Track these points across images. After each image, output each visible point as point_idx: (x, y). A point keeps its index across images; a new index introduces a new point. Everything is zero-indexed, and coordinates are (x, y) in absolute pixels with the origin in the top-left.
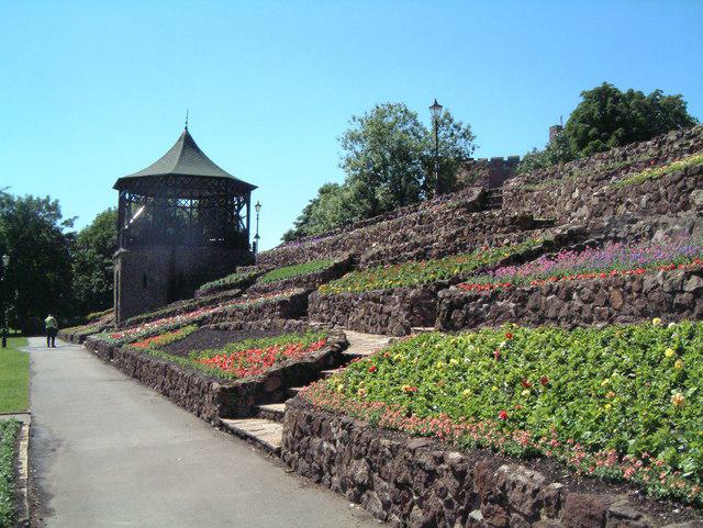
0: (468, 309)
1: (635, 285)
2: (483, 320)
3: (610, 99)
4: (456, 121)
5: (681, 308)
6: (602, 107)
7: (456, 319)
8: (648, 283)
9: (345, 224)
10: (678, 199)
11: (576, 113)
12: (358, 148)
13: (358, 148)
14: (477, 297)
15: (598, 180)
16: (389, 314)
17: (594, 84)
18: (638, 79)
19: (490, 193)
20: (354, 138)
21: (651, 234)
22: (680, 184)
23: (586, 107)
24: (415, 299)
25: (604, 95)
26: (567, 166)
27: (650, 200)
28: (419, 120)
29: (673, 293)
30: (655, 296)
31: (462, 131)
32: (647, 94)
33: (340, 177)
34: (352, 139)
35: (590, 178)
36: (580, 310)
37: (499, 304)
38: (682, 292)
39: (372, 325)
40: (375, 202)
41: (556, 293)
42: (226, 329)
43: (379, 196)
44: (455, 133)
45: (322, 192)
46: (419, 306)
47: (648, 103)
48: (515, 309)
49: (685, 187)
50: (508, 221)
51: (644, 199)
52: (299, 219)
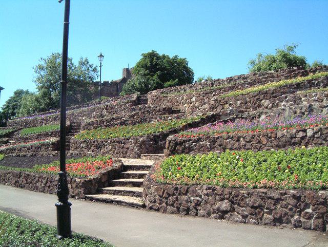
0: (185, 145)
1: (273, 135)
2: (193, 150)
3: (155, 58)
4: (90, 63)
5: (294, 144)
6: (151, 61)
7: (178, 150)
8: (279, 134)
9: (36, 109)
10: (256, 103)
11: (139, 63)
12: (42, 73)
13: (42, 73)
14: (190, 140)
15: (206, 94)
16: (128, 148)
17: (148, 50)
18: (168, 50)
19: (140, 97)
20: (41, 68)
21: (259, 116)
22: (257, 97)
23: (144, 61)
24: (143, 142)
25: (152, 56)
26: (183, 87)
27: (242, 103)
28: (73, 61)
29: (292, 138)
30: (284, 139)
31: (93, 68)
32: (171, 57)
33: (33, 88)
34: (40, 68)
35: (202, 93)
36: (245, 145)
37: (202, 143)
38: (295, 138)
39: (117, 153)
40: (51, 99)
41: (232, 138)
42: (24, 156)
43: (53, 96)
44: (90, 68)
45: (16, 93)
46: (145, 145)
47: (172, 61)
48: (210, 145)
49: (259, 98)
50: (162, 110)
51: (239, 103)
52: (4, 106)
